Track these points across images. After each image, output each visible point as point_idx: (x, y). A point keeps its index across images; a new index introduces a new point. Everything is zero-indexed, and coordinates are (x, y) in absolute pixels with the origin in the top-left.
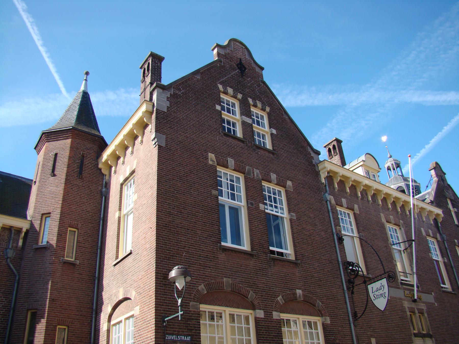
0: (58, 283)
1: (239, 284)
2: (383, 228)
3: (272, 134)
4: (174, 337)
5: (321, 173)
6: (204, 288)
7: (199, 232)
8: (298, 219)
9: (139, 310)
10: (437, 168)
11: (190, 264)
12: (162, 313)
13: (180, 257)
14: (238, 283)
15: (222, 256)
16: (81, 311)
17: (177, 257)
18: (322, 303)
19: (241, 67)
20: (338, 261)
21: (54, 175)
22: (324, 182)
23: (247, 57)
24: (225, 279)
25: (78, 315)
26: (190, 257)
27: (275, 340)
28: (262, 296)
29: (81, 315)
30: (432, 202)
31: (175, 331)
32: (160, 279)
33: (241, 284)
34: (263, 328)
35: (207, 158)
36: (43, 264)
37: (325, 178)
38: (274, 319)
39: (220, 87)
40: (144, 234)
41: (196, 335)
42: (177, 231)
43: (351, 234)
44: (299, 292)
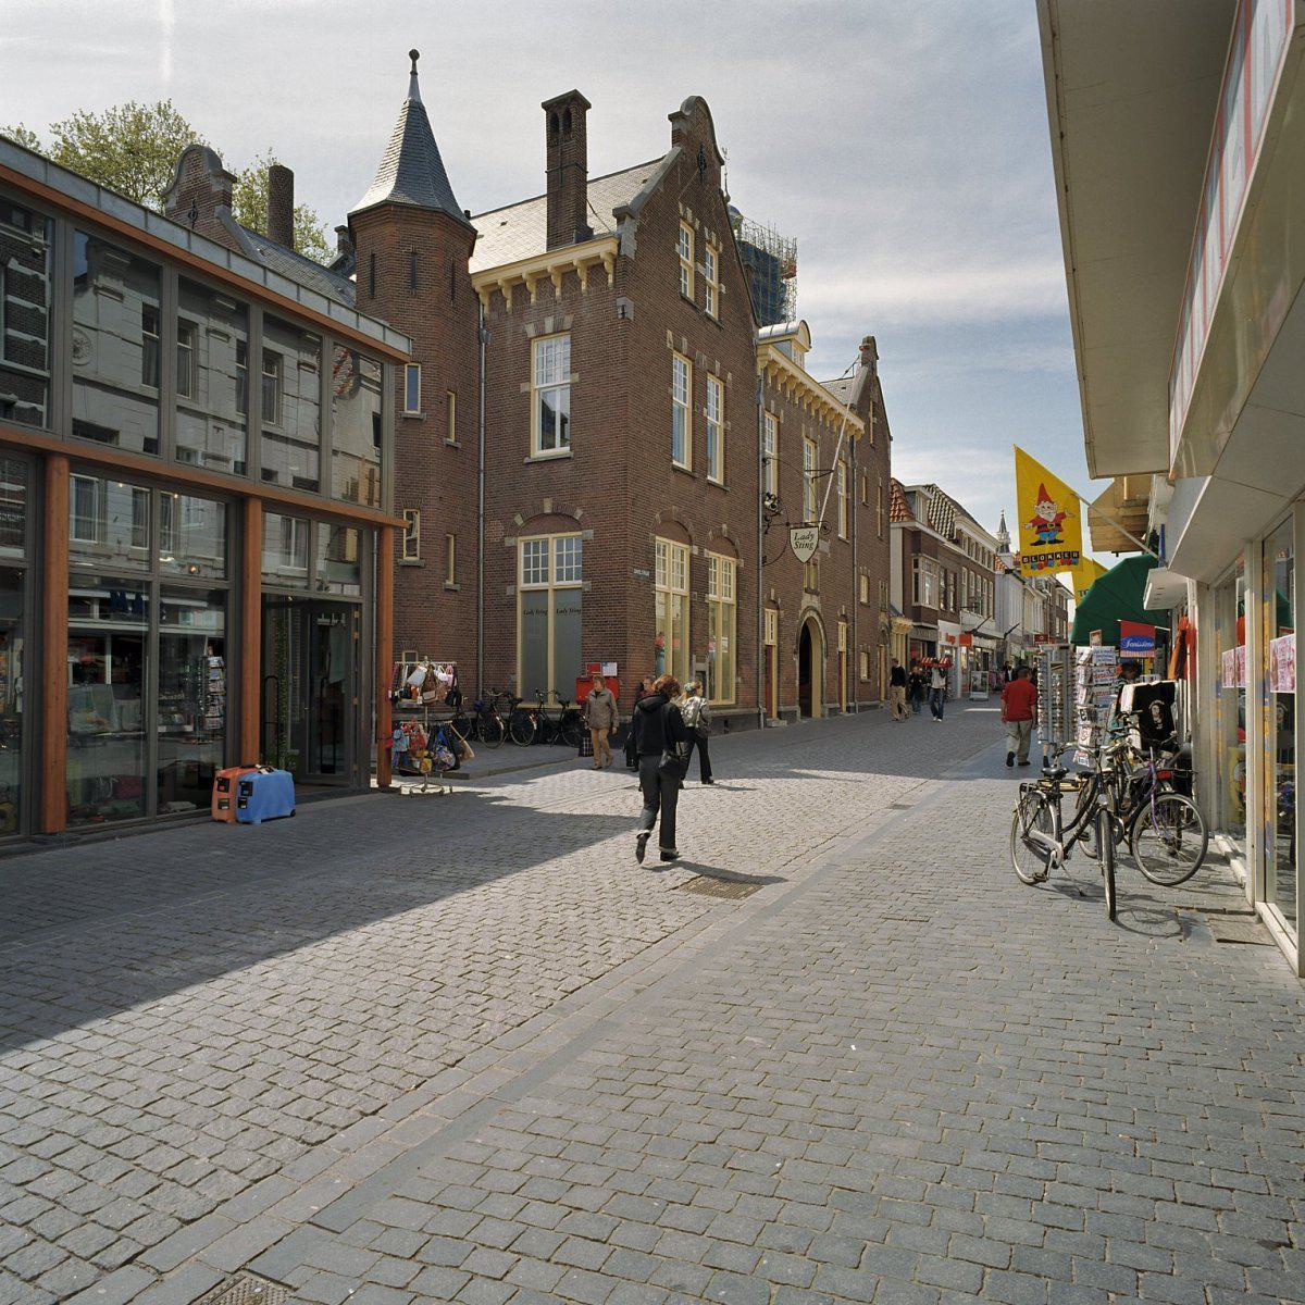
5: (758, 359)
10: (869, 348)
15: (672, 477)
30: (852, 407)
44: (724, 526)
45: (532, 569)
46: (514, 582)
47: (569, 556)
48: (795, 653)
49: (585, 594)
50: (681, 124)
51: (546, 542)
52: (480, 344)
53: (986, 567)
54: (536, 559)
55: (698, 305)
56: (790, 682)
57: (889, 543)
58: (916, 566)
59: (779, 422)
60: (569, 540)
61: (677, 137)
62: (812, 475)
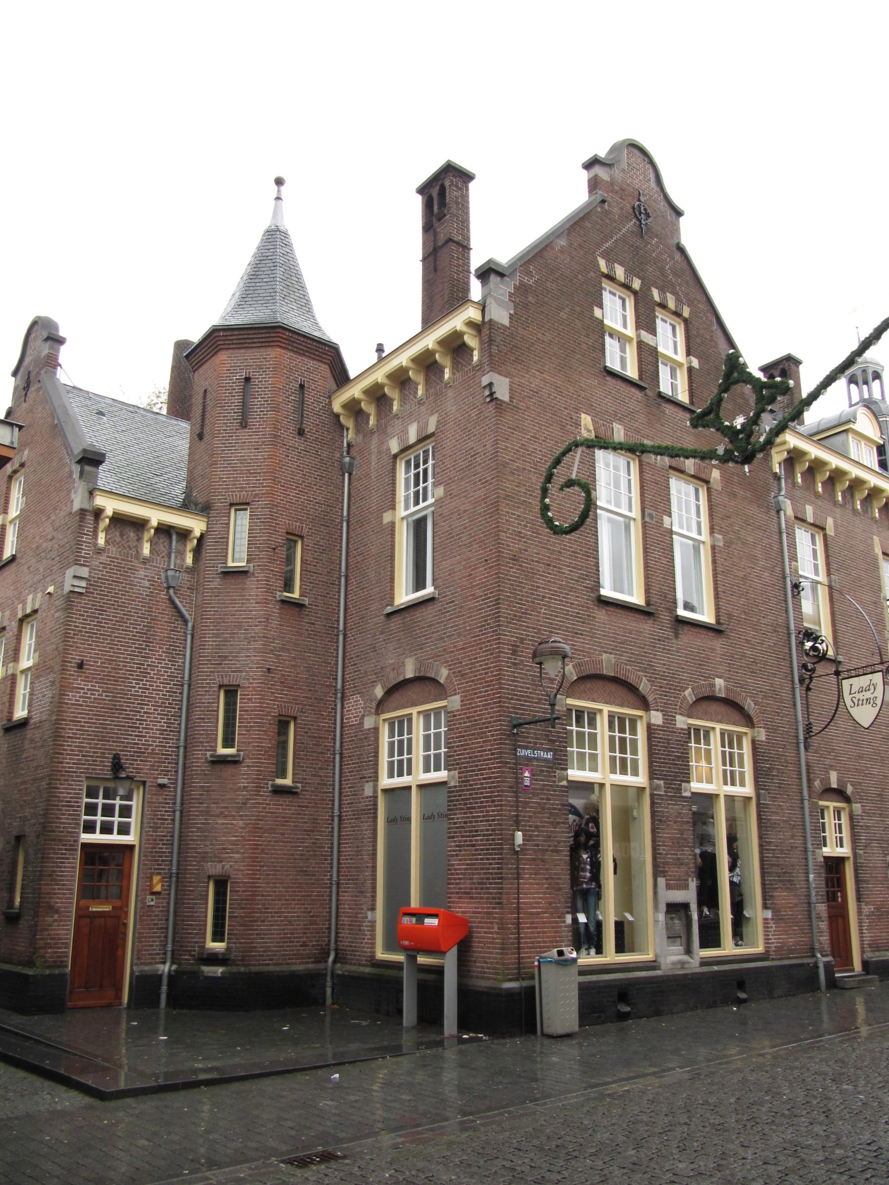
0: (274, 639)
1: (626, 664)
3: (690, 370)
4: (528, 753)
6: (573, 671)
7: (566, 570)
8: (728, 544)
9: (459, 703)
11: (552, 628)
12: (511, 712)
13: (537, 616)
14: (626, 664)
15: (601, 615)
16: (316, 691)
17: (531, 615)
18: (755, 704)
19: (639, 213)
20: (788, 628)
22: (778, 471)
23: (653, 184)
24: (605, 656)
25: (311, 698)
26: (551, 615)
27: (676, 764)
28: (661, 687)
29: (316, 699)
31: (530, 742)
32: (507, 653)
33: (630, 665)
34: (659, 742)
35: (578, 424)
36: (243, 603)
37: (780, 464)
38: (677, 729)
39: (602, 263)
40: (465, 568)
41: (561, 751)
42: (531, 568)
43: (694, 535)
46: (375, 778)
50: (598, 170)
51: (409, 717)
52: (343, 475)
59: (825, 536)
60: (437, 712)
61: (594, 184)
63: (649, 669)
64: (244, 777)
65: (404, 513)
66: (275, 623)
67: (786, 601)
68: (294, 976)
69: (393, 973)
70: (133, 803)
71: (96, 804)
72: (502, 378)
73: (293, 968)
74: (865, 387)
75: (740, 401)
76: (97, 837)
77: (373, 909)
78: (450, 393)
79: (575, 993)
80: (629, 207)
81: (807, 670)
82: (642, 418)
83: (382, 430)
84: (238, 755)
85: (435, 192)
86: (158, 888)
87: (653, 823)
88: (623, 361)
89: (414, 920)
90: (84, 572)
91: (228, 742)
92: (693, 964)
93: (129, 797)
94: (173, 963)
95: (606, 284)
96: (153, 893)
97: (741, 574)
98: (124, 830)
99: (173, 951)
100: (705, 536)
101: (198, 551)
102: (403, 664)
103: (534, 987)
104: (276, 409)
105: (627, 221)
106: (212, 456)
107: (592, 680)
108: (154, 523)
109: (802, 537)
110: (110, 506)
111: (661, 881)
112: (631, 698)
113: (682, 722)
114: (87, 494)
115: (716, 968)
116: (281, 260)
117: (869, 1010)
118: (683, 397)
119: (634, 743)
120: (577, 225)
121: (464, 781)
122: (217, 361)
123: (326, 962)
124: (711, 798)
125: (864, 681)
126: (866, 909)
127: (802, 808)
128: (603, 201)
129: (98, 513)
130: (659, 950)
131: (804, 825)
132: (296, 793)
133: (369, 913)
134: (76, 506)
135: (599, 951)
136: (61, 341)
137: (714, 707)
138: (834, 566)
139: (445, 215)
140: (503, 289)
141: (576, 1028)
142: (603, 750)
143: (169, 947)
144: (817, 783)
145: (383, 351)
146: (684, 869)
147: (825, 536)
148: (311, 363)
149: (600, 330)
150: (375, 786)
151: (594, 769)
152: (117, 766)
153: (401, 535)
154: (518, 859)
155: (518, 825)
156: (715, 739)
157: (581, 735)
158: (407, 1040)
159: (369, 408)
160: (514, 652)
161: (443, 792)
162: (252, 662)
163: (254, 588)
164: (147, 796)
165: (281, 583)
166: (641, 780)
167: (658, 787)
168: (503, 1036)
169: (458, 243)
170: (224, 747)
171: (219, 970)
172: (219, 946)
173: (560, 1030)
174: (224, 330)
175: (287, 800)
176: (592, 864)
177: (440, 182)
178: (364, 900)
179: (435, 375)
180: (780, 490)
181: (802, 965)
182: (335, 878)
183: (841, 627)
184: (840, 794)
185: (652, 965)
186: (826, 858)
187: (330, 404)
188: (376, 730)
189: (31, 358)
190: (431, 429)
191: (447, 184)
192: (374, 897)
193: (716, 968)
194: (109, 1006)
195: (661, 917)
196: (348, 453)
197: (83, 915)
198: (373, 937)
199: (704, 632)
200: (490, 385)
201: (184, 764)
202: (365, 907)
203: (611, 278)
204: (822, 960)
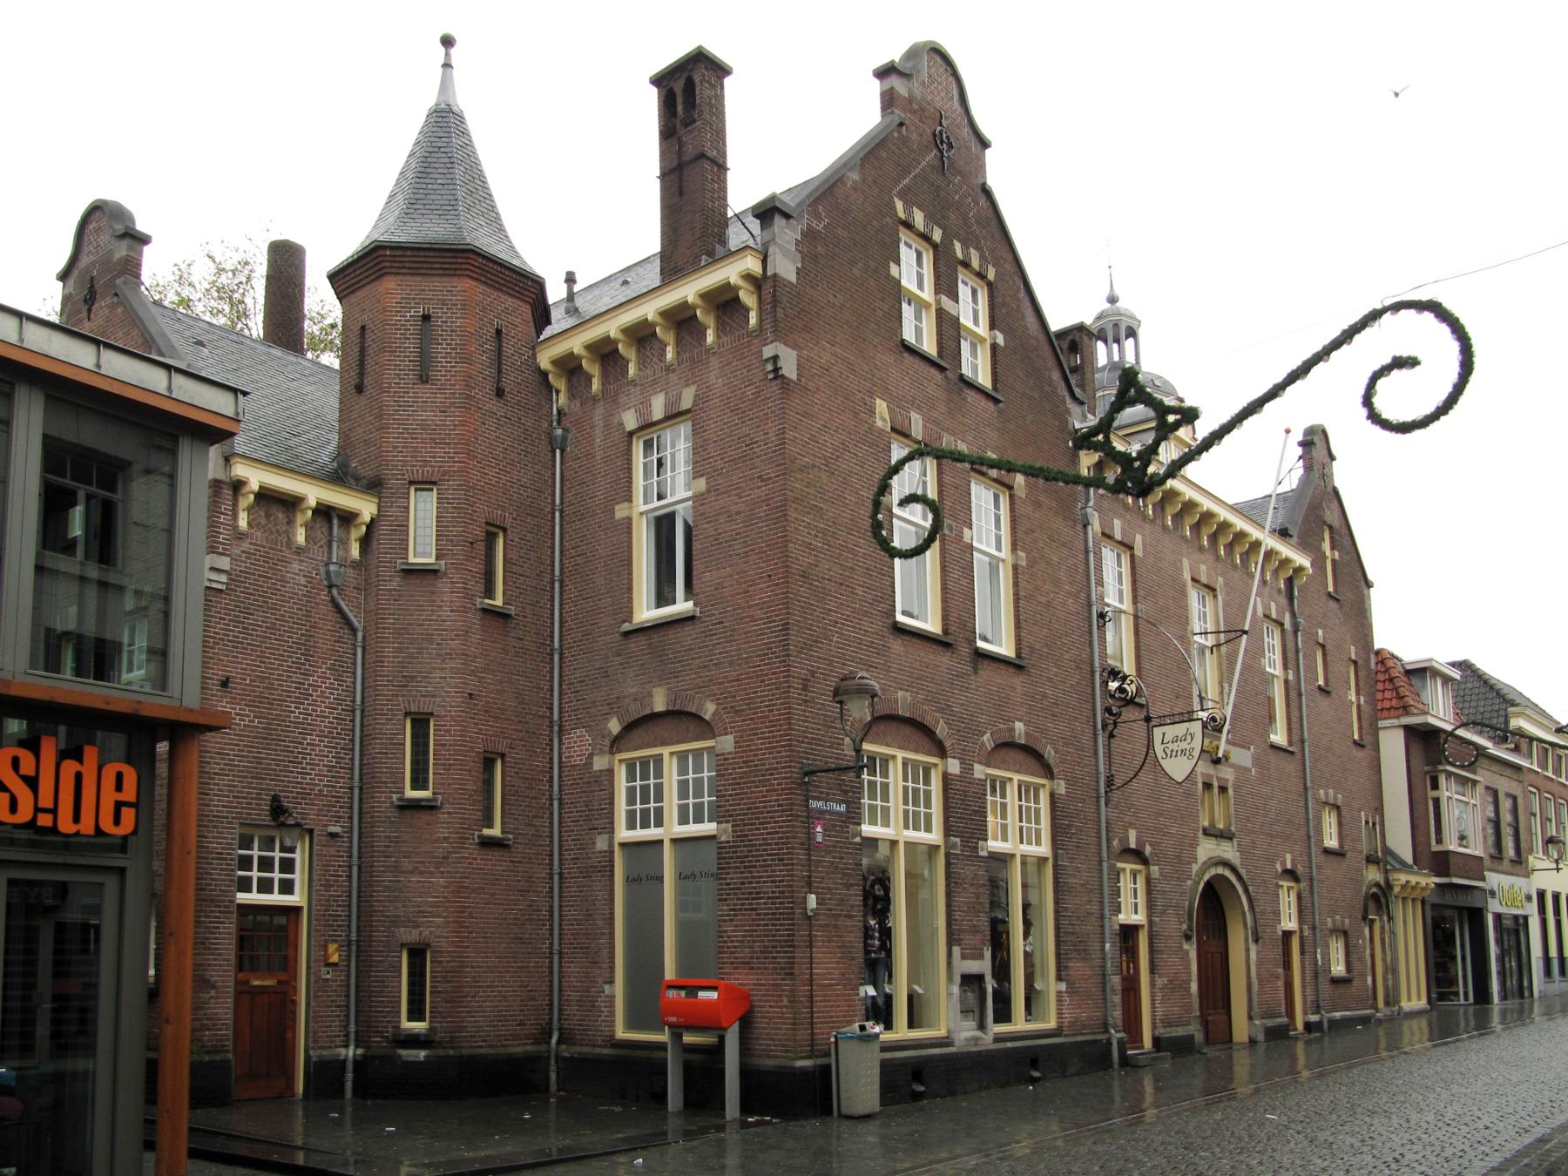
2: (1183, 594)
3: (994, 347)
8: (1032, 563)
15: (897, 645)
19: (939, 141)
20: (1092, 665)
21: (424, 379)
23: (956, 104)
24: (900, 693)
39: (899, 205)
43: (993, 552)
45: (879, 803)
46: (610, 829)
47: (698, 783)
48: (1188, 938)
49: (721, 847)
50: (895, 82)
51: (659, 760)
52: (554, 452)
53: (1550, 774)
54: (645, 789)
55: (945, 362)
56: (1182, 986)
57: (1378, 750)
58: (1435, 786)
59: (1132, 556)
60: (698, 753)
61: (889, 101)
62: (1210, 641)
63: (945, 710)
64: (443, 827)
65: (643, 508)
66: (476, 638)
67: (1090, 633)
68: (511, 1060)
69: (657, 1055)
70: (297, 856)
71: (251, 857)
72: (789, 350)
73: (511, 1050)
74: (1115, 346)
75: (1047, 388)
76: (254, 897)
77: (611, 982)
78: (714, 362)
79: (877, 1071)
80: (929, 132)
81: (1111, 713)
82: (942, 407)
83: (611, 397)
84: (434, 800)
85: (678, 87)
86: (335, 958)
87: (948, 886)
88: (918, 331)
89: (683, 993)
90: (224, 563)
91: (419, 782)
92: (987, 1041)
93: (292, 850)
94: (357, 1046)
95: (904, 235)
96: (328, 965)
97: (1044, 600)
98: (287, 887)
99: (357, 1033)
100: (1005, 553)
101: (365, 542)
102: (650, 695)
103: (829, 1066)
104: (467, 360)
105: (924, 149)
106: (380, 417)
107: (886, 721)
108: (312, 503)
109: (1109, 555)
110: (255, 478)
111: (956, 950)
112: (926, 742)
113: (980, 771)
114: (221, 461)
115: (1009, 1045)
116: (458, 155)
117: (1158, 1089)
118: (984, 379)
119: (928, 794)
120: (873, 154)
121: (740, 836)
122: (381, 289)
123: (549, 1043)
124: (1003, 859)
125: (1180, 729)
126: (1160, 982)
127: (1100, 871)
128: (901, 124)
129: (238, 486)
130: (951, 1025)
131: (1101, 888)
132: (507, 846)
133: (607, 987)
134: (211, 476)
135: (889, 1026)
136: (144, 240)
137: (1013, 755)
138: (1141, 592)
139: (694, 121)
140: (786, 235)
141: (878, 1109)
142: (896, 803)
143: (352, 1028)
144: (1115, 843)
145: (574, 282)
146: (979, 936)
147: (1132, 556)
148: (510, 302)
149: (895, 292)
150: (611, 840)
151: (886, 824)
152: (278, 810)
153: (640, 538)
154: (811, 925)
155: (810, 886)
156: (1012, 791)
157: (872, 784)
158: (674, 1124)
159: (592, 368)
160: (805, 688)
161: (712, 847)
162: (449, 685)
163: (447, 593)
164: (316, 848)
165: (480, 587)
166: (935, 836)
167: (954, 846)
168: (795, 1117)
169: (713, 161)
170: (413, 788)
171: (422, 1054)
172: (419, 1026)
173: (861, 1110)
174: (391, 248)
175: (498, 853)
176: (880, 932)
177: (685, 75)
178: (598, 971)
179: (690, 334)
180: (1088, 500)
181: (1096, 1041)
182: (556, 946)
183: (1146, 665)
184: (1138, 855)
185: (946, 1042)
186: (1122, 926)
187: (534, 356)
188: (610, 772)
189: (92, 258)
190: (686, 403)
191: (697, 78)
192: (612, 968)
193: (1009, 1045)
194: (280, 1097)
195: (956, 989)
196: (559, 422)
197: (243, 992)
198: (612, 1014)
199: (1003, 667)
200: (775, 358)
201: (360, 809)
202: (600, 980)
203: (908, 225)
204: (1116, 1035)
